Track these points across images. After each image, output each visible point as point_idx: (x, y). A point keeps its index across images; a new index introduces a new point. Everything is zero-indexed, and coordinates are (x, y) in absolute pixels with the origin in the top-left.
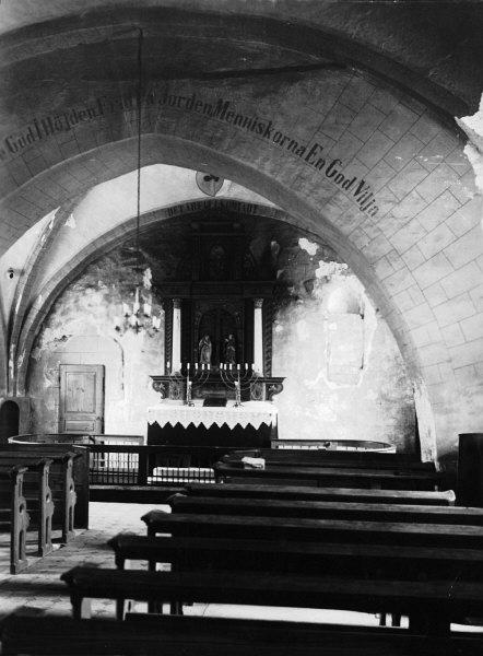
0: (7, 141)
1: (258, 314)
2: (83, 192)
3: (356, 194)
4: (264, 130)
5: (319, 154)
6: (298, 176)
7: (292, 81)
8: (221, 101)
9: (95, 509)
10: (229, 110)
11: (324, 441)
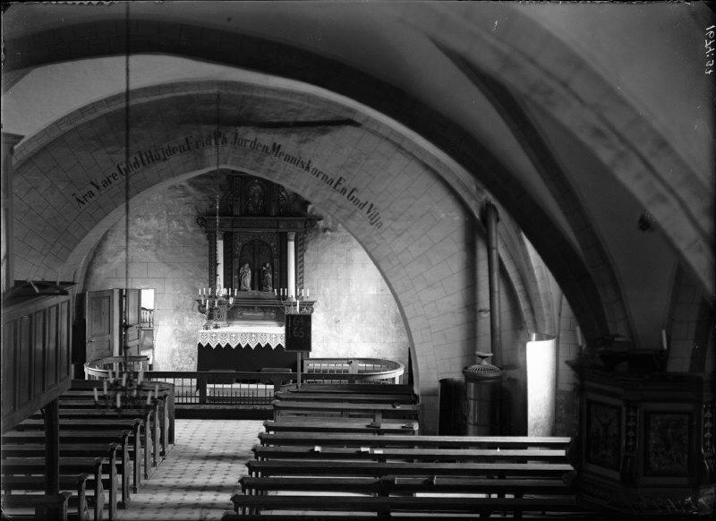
0: (118, 167)
1: (291, 245)
2: (270, 319)
3: (369, 212)
4: (305, 166)
5: (343, 184)
6: (329, 199)
7: (324, 132)
8: (275, 144)
9: (180, 425)
10: (281, 151)
11: (348, 359)
